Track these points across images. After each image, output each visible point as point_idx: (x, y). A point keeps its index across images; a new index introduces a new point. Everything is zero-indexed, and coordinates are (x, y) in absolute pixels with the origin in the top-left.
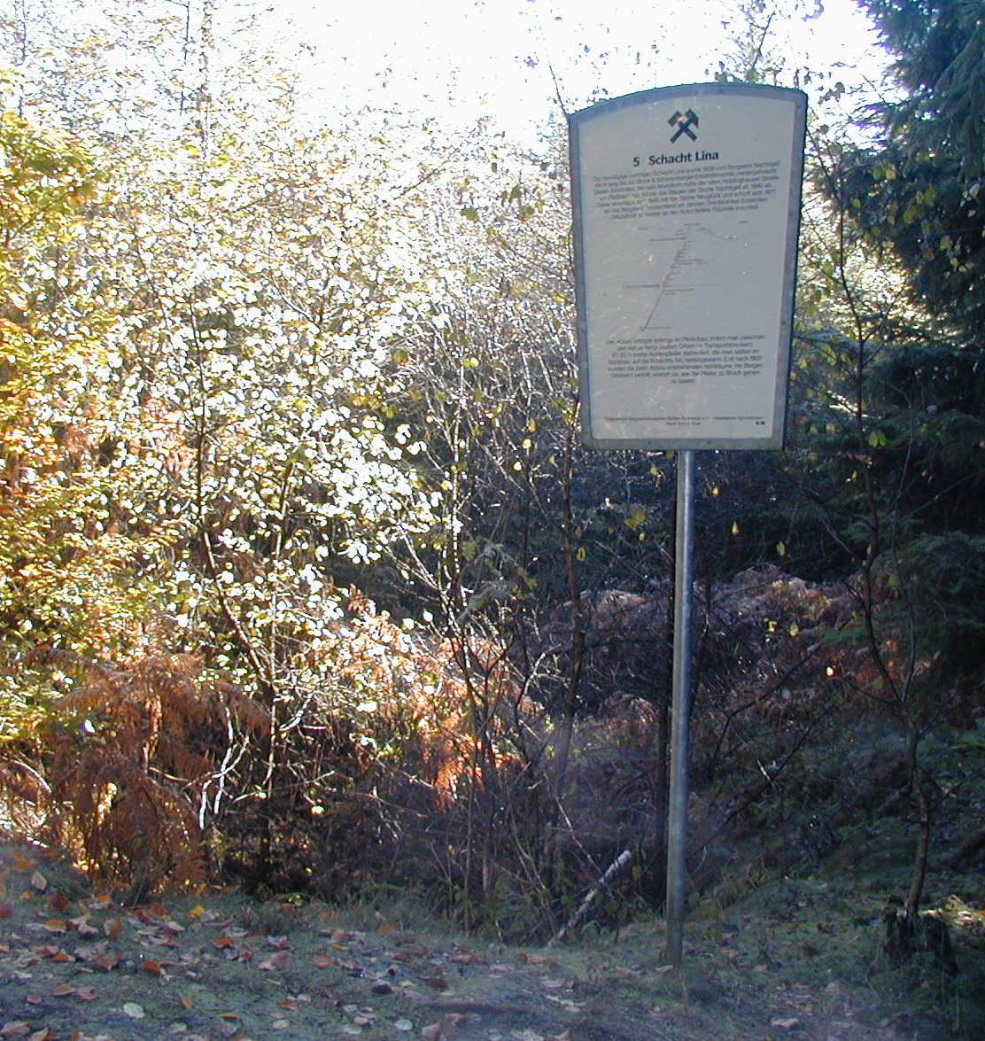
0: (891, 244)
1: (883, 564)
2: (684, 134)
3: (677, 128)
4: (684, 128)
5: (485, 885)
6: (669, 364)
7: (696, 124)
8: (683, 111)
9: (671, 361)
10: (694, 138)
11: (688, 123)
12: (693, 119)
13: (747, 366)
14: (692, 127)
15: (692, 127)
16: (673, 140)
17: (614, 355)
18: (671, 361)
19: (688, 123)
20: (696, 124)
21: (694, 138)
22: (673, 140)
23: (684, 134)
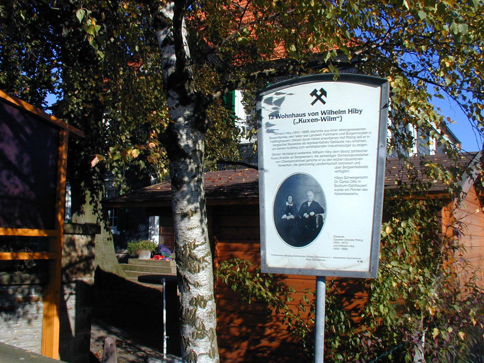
0: (143, 154)
1: (222, 149)
2: (319, 101)
3: (315, 98)
4: (319, 98)
5: (24, 139)
6: (353, 139)
7: (326, 96)
8: (318, 89)
9: (308, 143)
10: (324, 102)
11: (321, 95)
12: (324, 92)
13: (289, 144)
14: (323, 97)
15: (323, 97)
16: (313, 104)
17: (368, 137)
18: (308, 143)
19: (321, 95)
20: (326, 96)
21: (324, 102)
22: (313, 104)
23: (319, 101)
